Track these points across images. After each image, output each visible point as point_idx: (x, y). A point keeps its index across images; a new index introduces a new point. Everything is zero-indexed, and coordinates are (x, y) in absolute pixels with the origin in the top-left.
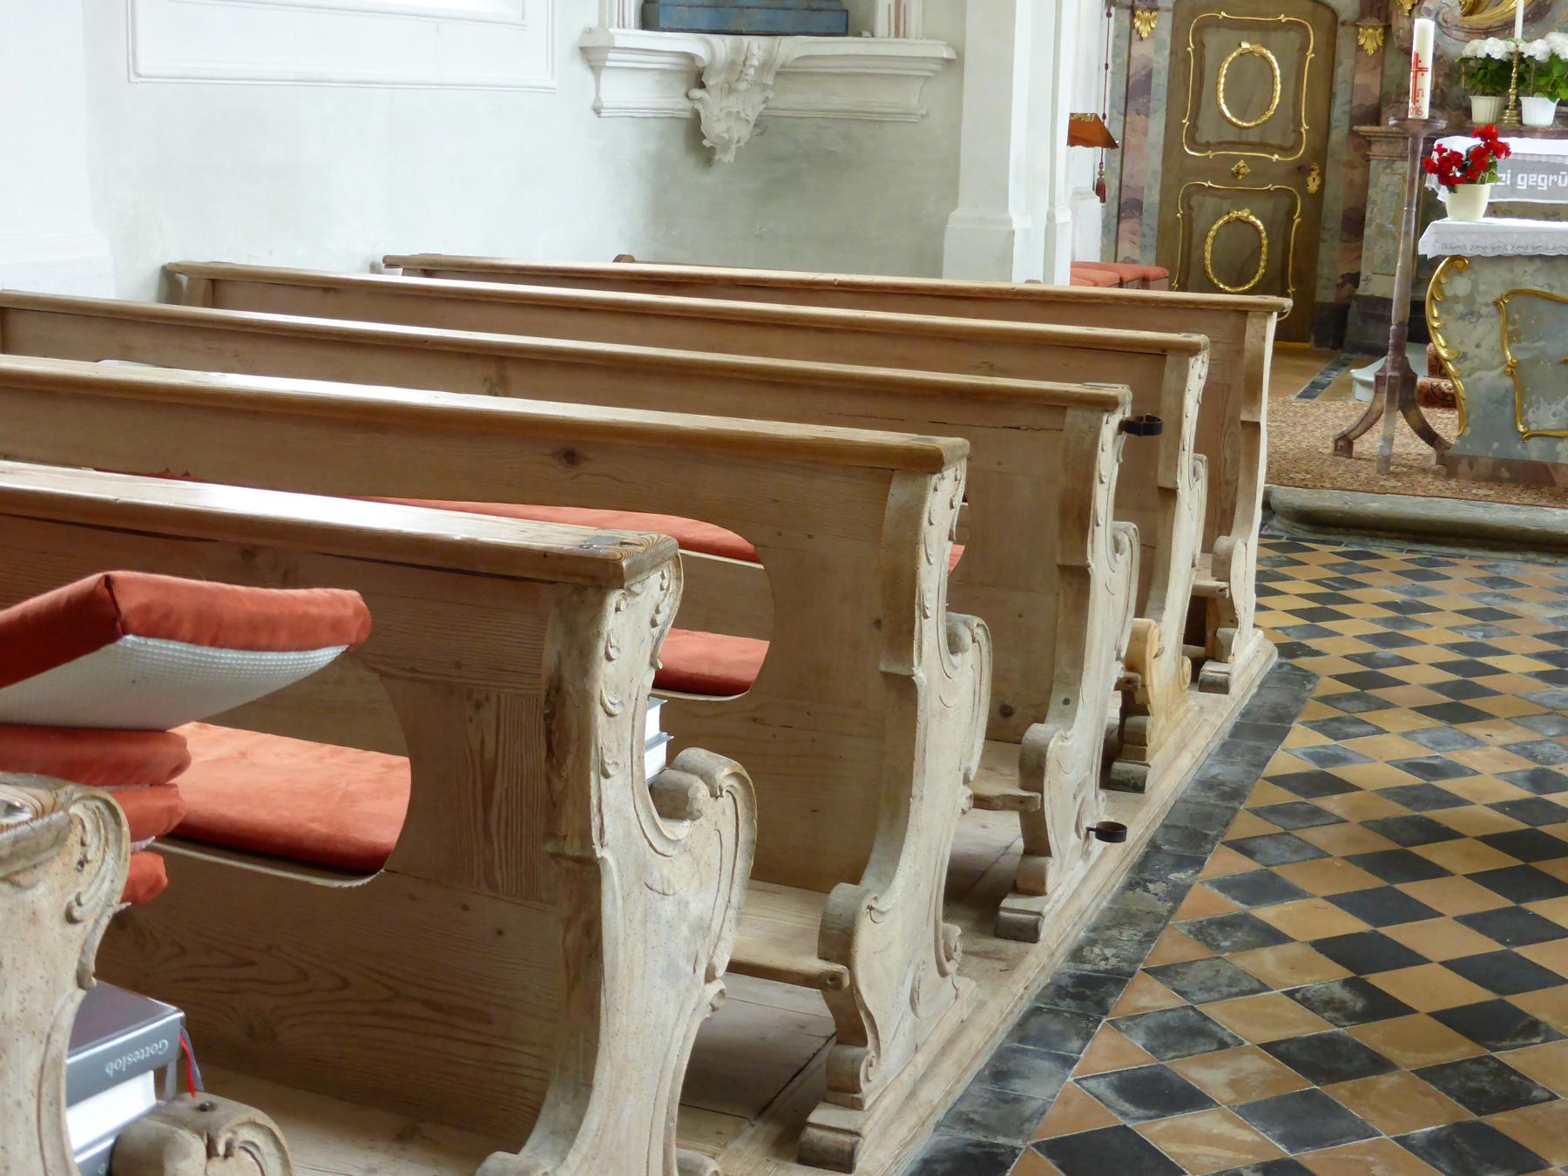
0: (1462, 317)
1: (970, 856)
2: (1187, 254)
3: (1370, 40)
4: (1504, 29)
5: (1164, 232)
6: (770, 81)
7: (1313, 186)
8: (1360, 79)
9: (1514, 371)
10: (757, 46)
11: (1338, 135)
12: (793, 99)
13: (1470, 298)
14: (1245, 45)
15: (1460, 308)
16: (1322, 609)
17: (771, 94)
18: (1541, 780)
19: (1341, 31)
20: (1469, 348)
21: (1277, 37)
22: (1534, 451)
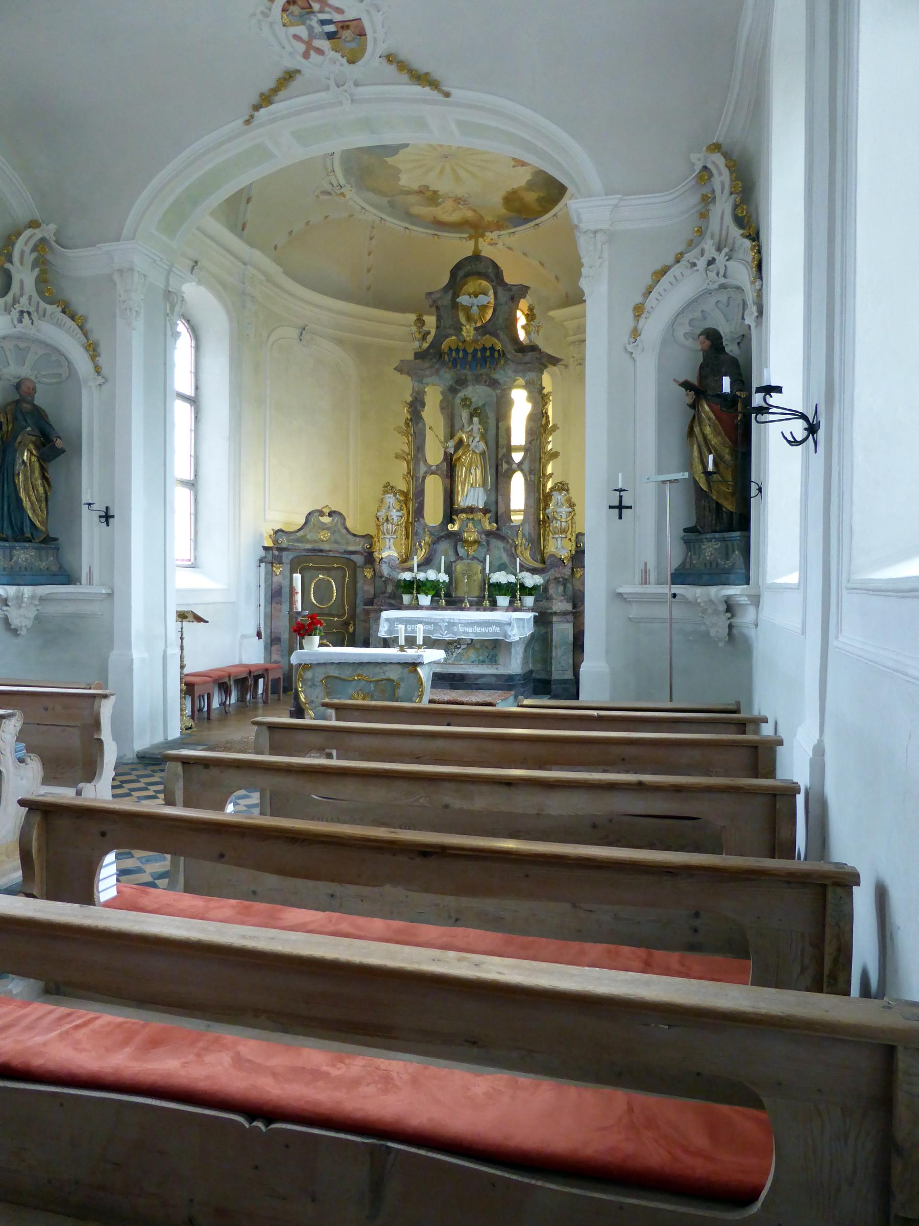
0: (311, 687)
1: (744, 1013)
4: (411, 569)
6: (37, 602)
7: (351, 630)
8: (366, 588)
10: (27, 590)
11: (359, 610)
12: (50, 609)
13: (313, 679)
14: (321, 576)
15: (309, 683)
17: (39, 608)
19: (358, 570)
20: (313, 698)
21: (333, 573)
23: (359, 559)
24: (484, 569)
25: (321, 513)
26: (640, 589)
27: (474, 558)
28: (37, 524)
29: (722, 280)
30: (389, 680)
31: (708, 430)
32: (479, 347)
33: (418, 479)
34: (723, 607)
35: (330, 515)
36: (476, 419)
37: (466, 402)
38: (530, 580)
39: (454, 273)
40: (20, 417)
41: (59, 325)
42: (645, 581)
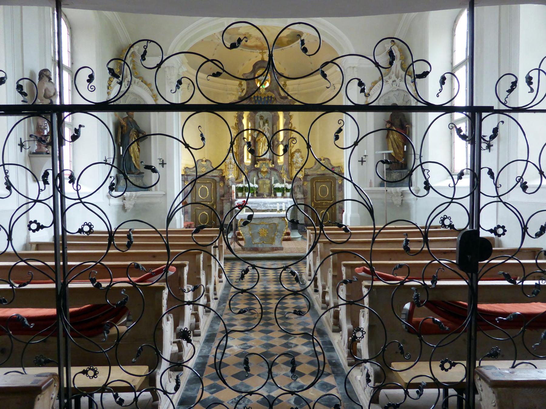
2: (196, 219)
3: (222, 184)
5: (192, 217)
7: (215, 207)
8: (221, 190)
9: (251, 235)
10: (134, 193)
11: (218, 199)
12: (139, 201)
16: (231, 271)
18: (265, 288)
21: (207, 184)
22: (255, 246)
23: (217, 179)
24: (271, 182)
25: (202, 161)
26: (370, 189)
27: (267, 178)
28: (137, 167)
29: (398, 88)
30: (275, 224)
31: (395, 137)
32: (266, 96)
33: (241, 147)
34: (400, 194)
35: (206, 161)
36: (266, 124)
37: (261, 118)
38: (289, 186)
39: (254, 66)
40: (129, 124)
41: (140, 86)
42: (371, 186)
